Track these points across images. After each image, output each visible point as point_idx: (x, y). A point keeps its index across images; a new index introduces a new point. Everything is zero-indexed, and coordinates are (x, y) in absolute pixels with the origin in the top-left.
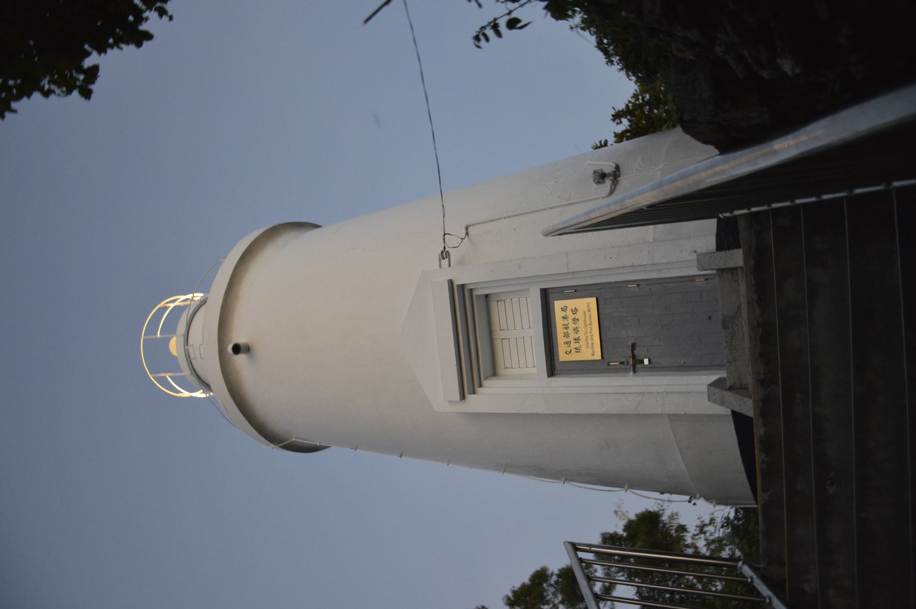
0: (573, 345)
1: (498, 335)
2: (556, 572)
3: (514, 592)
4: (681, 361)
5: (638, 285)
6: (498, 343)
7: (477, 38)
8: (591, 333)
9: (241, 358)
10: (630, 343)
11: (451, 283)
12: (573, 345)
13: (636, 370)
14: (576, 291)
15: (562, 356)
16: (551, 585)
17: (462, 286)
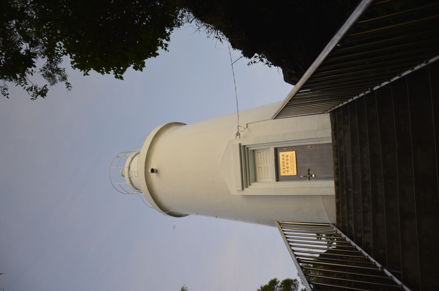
0: (286, 169)
1: (258, 166)
2: (281, 282)
3: (261, 287)
4: (327, 176)
5: (311, 147)
6: (257, 169)
7: (248, 64)
8: (293, 165)
9: (153, 175)
10: (307, 169)
11: (240, 145)
12: (286, 169)
13: (310, 179)
14: (288, 149)
15: (282, 174)
16: (278, 287)
17: (244, 146)
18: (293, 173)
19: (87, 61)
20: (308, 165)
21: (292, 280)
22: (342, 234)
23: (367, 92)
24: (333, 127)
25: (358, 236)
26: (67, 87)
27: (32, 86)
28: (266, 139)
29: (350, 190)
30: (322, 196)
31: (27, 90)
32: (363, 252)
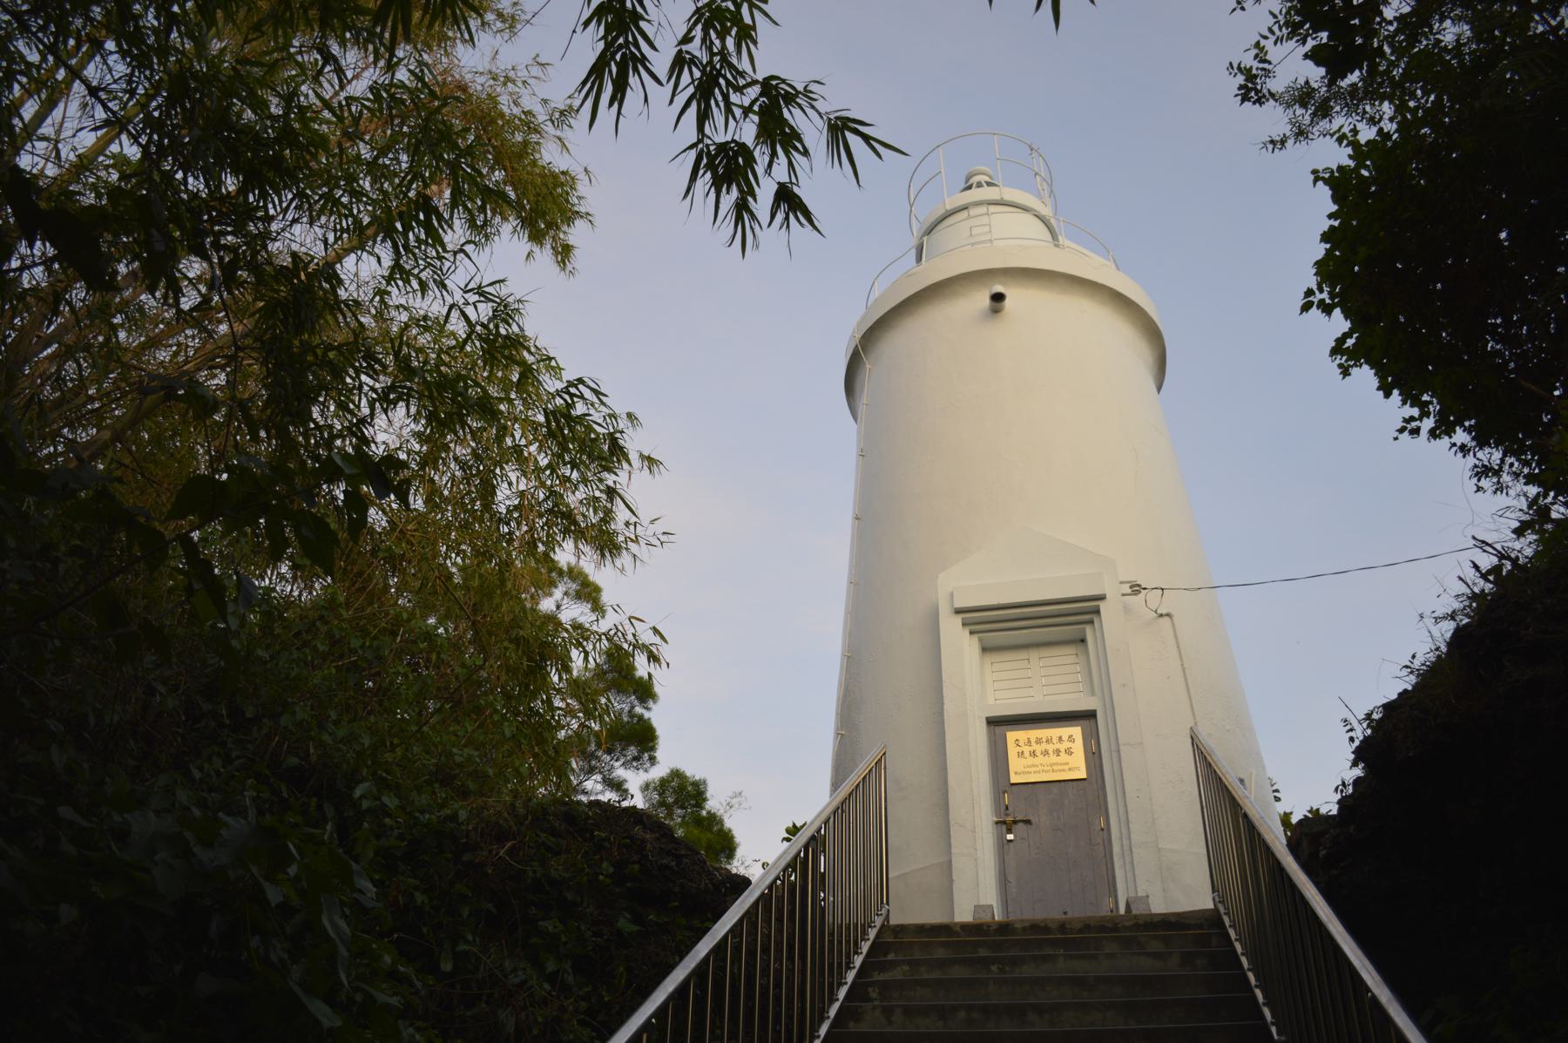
0: (1027, 749)
1: (1034, 655)
2: (647, 715)
4: (1012, 878)
5: (1102, 830)
6: (1023, 654)
7: (1346, 721)
9: (982, 299)
10: (1031, 818)
11: (1102, 598)
12: (1027, 749)
15: (1013, 736)
16: (633, 707)
17: (1097, 612)
18: (1016, 773)
19: (1354, 223)
20: (1042, 818)
21: (653, 749)
22: (869, 943)
23: (1274, 1030)
24: (1173, 920)
25: (870, 989)
26: (1272, 142)
27: (1270, 63)
28: (1124, 686)
29: (994, 968)
30: (950, 862)
31: (1258, 43)
32: (836, 1006)
